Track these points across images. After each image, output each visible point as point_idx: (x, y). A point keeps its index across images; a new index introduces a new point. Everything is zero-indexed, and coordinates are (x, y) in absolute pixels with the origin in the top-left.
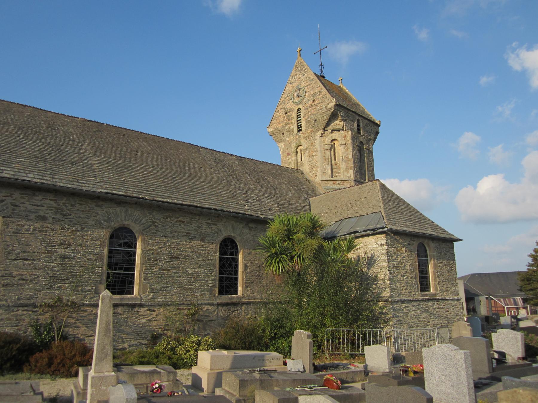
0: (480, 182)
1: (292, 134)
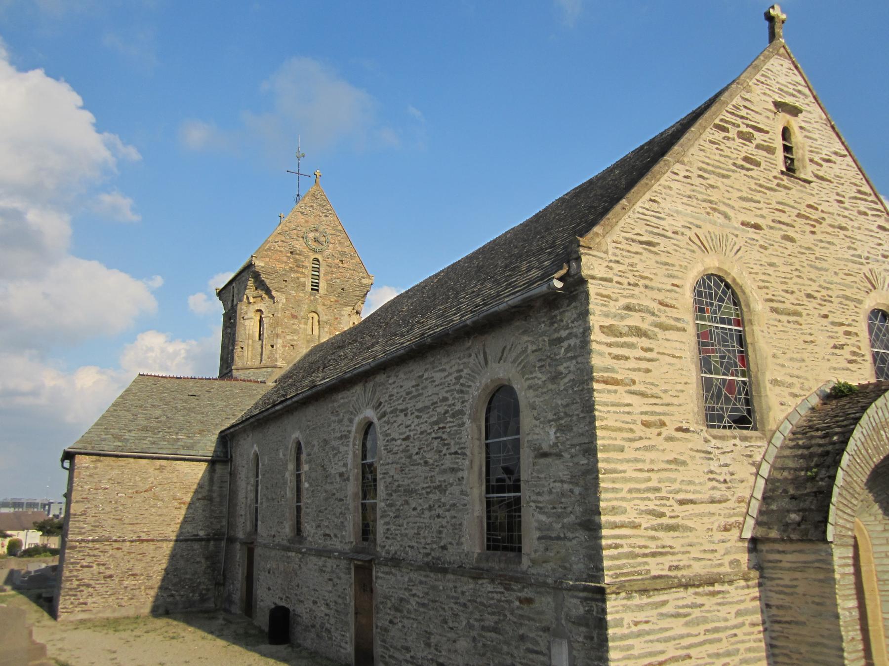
1: (303, 290)
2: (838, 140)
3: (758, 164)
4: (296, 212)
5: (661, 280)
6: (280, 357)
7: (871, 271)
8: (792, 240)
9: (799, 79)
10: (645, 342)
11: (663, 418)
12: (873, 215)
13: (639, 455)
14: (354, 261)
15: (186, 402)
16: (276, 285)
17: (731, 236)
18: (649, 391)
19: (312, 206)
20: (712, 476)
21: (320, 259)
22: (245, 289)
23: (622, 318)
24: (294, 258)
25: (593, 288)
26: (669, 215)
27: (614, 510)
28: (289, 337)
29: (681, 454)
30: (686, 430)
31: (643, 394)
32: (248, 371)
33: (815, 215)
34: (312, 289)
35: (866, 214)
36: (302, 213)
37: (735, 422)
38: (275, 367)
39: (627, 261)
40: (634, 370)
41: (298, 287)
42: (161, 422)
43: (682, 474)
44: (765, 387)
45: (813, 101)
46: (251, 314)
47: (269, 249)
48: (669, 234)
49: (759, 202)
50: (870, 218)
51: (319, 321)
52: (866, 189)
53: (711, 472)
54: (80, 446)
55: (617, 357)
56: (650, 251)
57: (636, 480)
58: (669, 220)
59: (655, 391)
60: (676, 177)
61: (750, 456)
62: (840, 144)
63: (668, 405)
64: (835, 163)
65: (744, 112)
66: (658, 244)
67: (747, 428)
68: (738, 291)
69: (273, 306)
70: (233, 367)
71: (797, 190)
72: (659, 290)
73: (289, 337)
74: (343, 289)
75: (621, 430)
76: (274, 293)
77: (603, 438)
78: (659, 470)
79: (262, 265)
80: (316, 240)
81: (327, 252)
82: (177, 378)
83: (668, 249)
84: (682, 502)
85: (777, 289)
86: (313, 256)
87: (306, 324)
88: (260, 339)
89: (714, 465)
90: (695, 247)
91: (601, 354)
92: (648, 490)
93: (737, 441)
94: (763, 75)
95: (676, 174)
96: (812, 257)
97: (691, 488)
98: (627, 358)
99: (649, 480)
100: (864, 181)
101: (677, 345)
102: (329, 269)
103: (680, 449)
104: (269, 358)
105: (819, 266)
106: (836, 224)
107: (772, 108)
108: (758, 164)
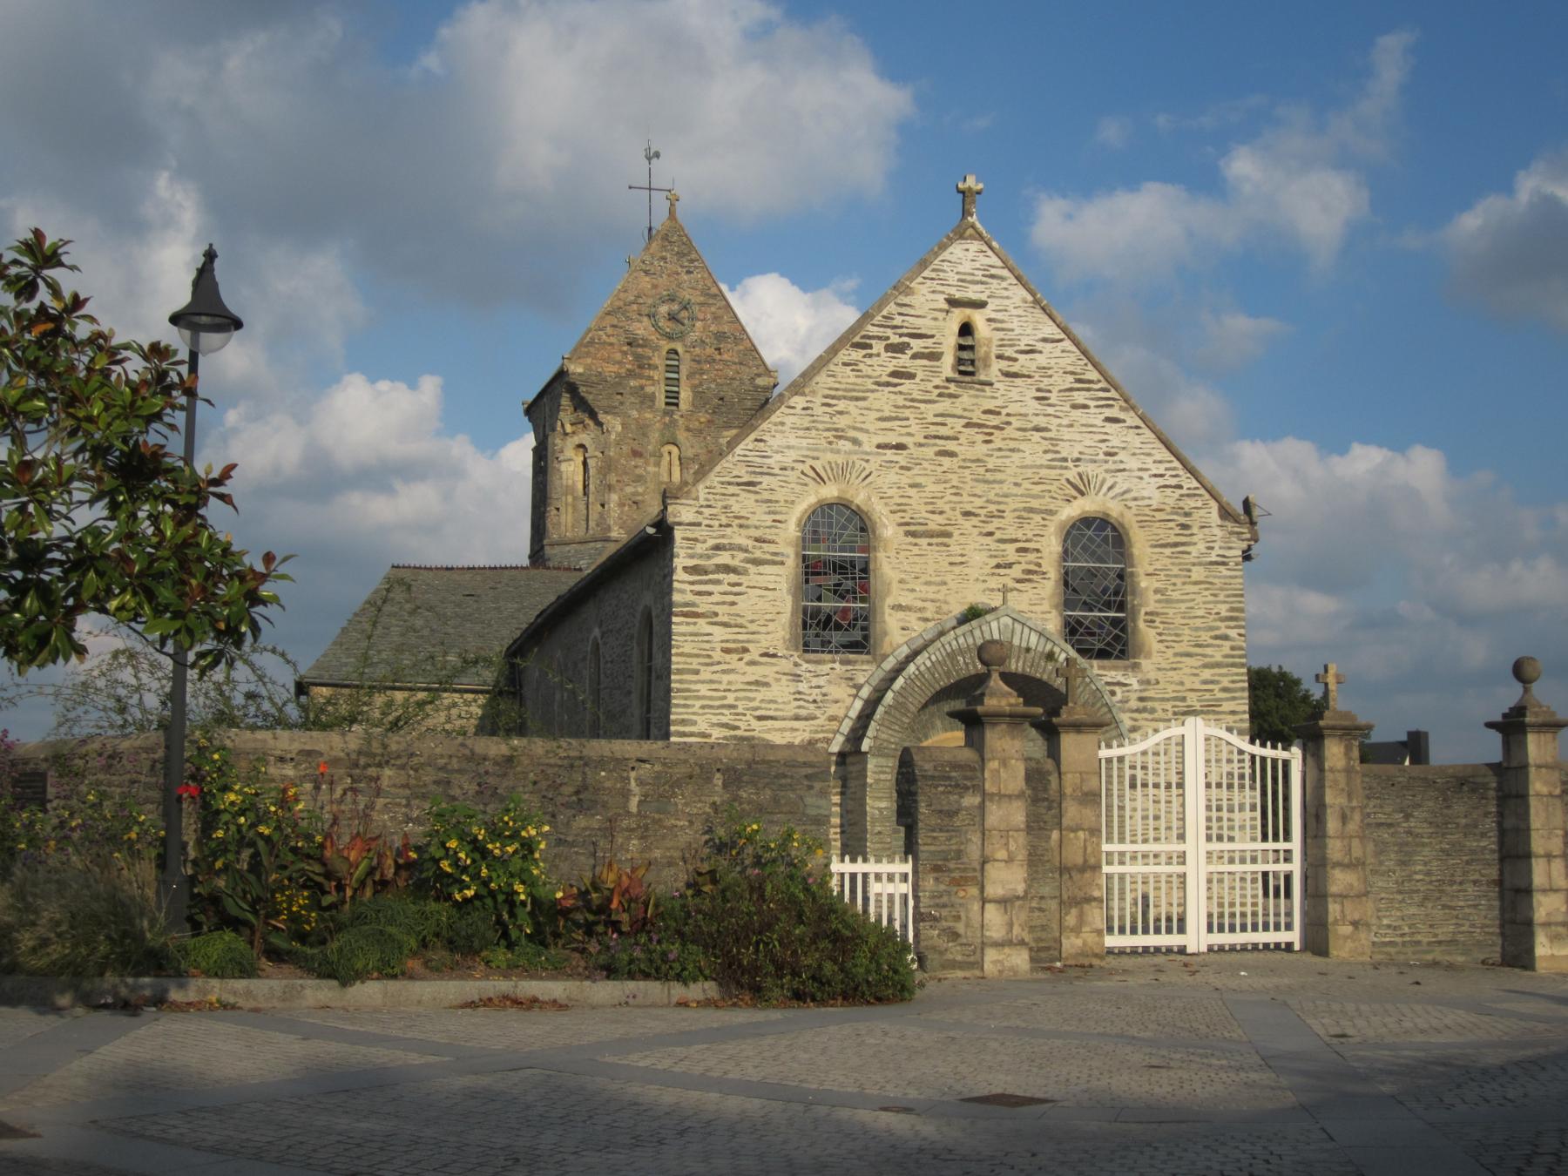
0: (785, 281)
1: (650, 407)
2: (1051, 323)
3: (911, 376)
4: (636, 271)
5: (760, 516)
6: (615, 523)
7: (1080, 475)
8: (952, 454)
9: (995, 260)
10: (733, 578)
11: (746, 645)
12: (1097, 407)
13: (715, 677)
14: (741, 348)
15: (459, 605)
16: (605, 403)
17: (858, 463)
18: (733, 622)
19: (664, 258)
20: (798, 696)
21: (680, 350)
22: (558, 411)
23: (709, 557)
24: (633, 354)
25: (678, 534)
26: (777, 452)
27: (683, 722)
28: (629, 490)
29: (765, 676)
30: (774, 656)
31: (725, 625)
32: (567, 548)
33: (994, 420)
34: (667, 404)
35: (1085, 407)
36: (646, 273)
37: (844, 646)
38: (607, 540)
39: (720, 504)
40: (717, 604)
41: (642, 403)
42: (422, 637)
43: (764, 693)
44: (883, 613)
45: (1015, 282)
46: (569, 452)
47: (592, 343)
48: (776, 471)
49: (908, 419)
50: (1093, 410)
51: (680, 459)
52: (1093, 375)
53: (799, 693)
54: (314, 673)
55: (699, 593)
56: (749, 491)
57: (711, 698)
58: (778, 457)
59: (740, 620)
60: (792, 411)
61: (851, 679)
62: (1055, 327)
63: (753, 633)
64: (1041, 352)
65: (898, 321)
66: (760, 483)
67: (862, 653)
68: (864, 517)
69: (602, 438)
70: (545, 542)
71: (970, 396)
72: (756, 527)
73: (629, 490)
74: (722, 399)
75: (697, 656)
76: (602, 417)
77: (678, 663)
78: (736, 691)
79: (580, 370)
80: (672, 317)
81: (693, 336)
82: (447, 569)
83: (772, 487)
84: (760, 718)
85: (918, 508)
86: (666, 345)
87: (658, 464)
88: (585, 494)
89: (803, 687)
90: (807, 480)
91: (682, 591)
92: (723, 706)
93: (837, 666)
94: (934, 270)
95: (793, 408)
96: (982, 471)
97: (773, 706)
98: (710, 594)
99: (725, 698)
100: (1090, 367)
101: (772, 578)
102: (695, 365)
103: (764, 671)
104: (598, 525)
105: (991, 478)
106: (1030, 425)
107: (946, 306)
108: (911, 376)
